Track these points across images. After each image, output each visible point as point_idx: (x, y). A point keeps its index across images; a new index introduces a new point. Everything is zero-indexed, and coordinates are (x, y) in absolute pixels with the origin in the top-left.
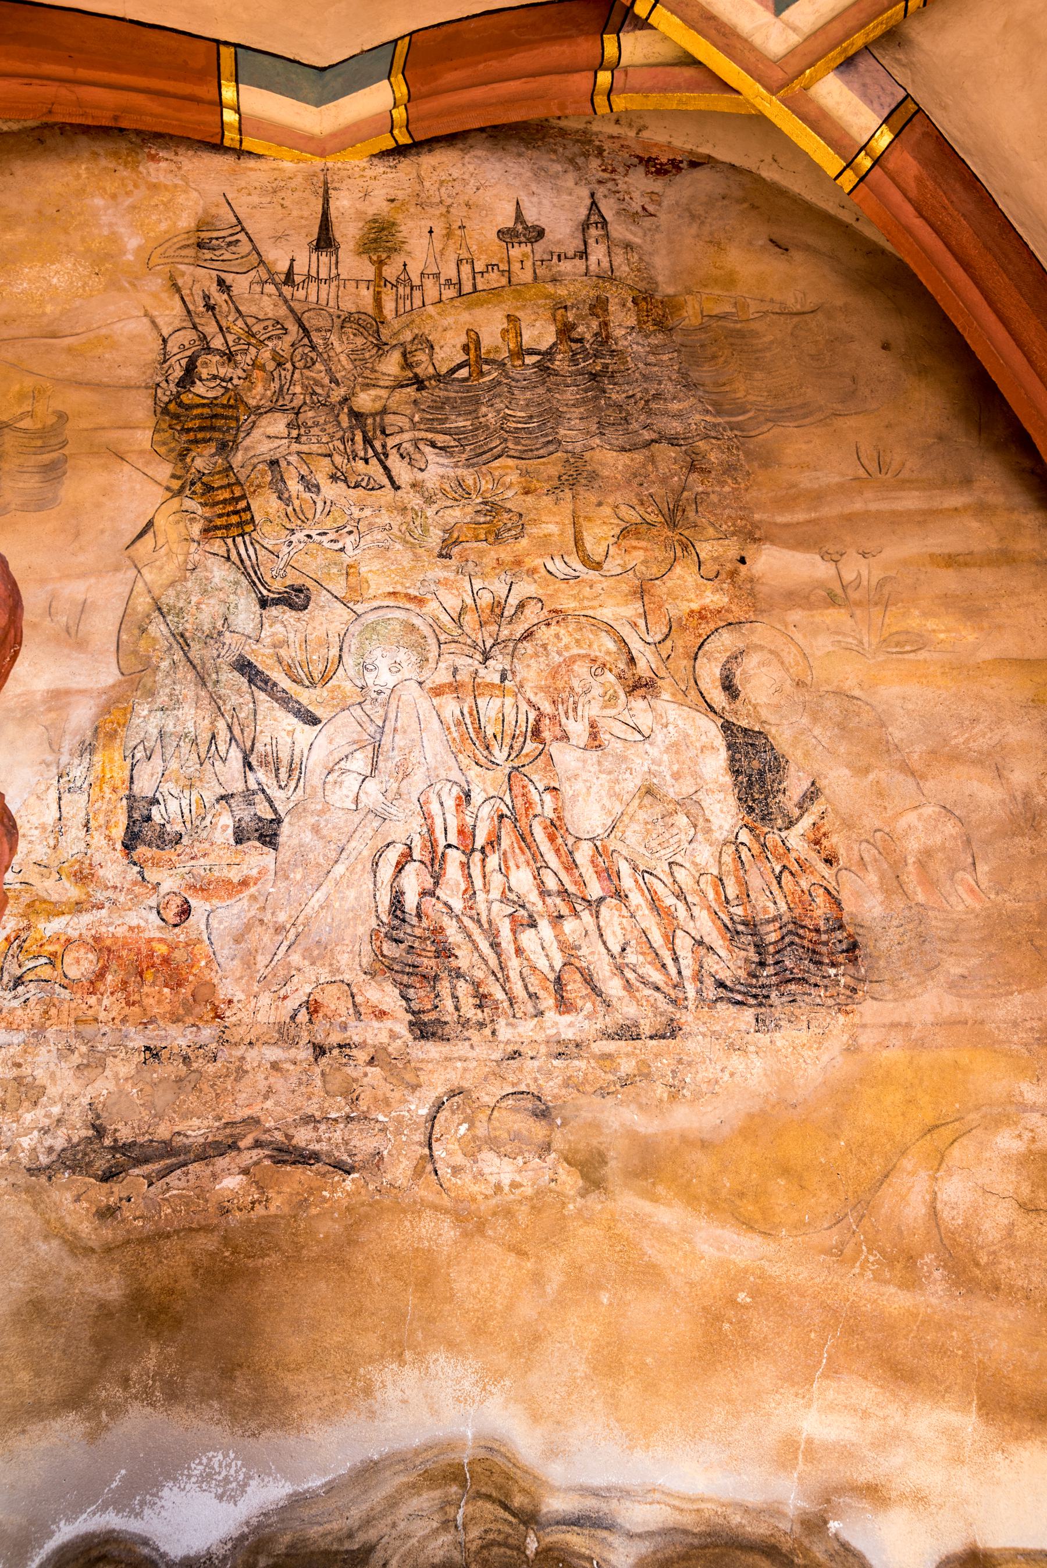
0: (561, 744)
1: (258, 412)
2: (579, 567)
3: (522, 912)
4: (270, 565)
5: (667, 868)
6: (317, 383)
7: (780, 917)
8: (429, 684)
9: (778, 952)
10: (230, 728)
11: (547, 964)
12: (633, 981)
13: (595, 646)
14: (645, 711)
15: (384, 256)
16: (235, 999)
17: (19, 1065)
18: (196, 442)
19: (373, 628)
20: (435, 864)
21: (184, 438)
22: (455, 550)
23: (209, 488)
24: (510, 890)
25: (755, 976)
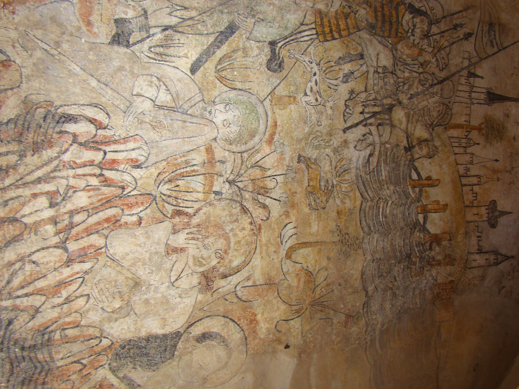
0: (170, 229)
1: (393, 49)
2: (288, 245)
3: (60, 199)
4: (297, 49)
5: (85, 293)
6: (410, 86)
7: (53, 361)
8: (214, 145)
9: (30, 359)
10: (191, 18)
11: (27, 213)
12: (14, 267)
13: (235, 253)
14: (191, 284)
15: (484, 132)
16: (15, 16)
18: (376, 11)
19: (254, 110)
20: (93, 144)
21: (378, 5)
22: (303, 166)
23: (347, 16)
24: (75, 192)
25: (15, 344)
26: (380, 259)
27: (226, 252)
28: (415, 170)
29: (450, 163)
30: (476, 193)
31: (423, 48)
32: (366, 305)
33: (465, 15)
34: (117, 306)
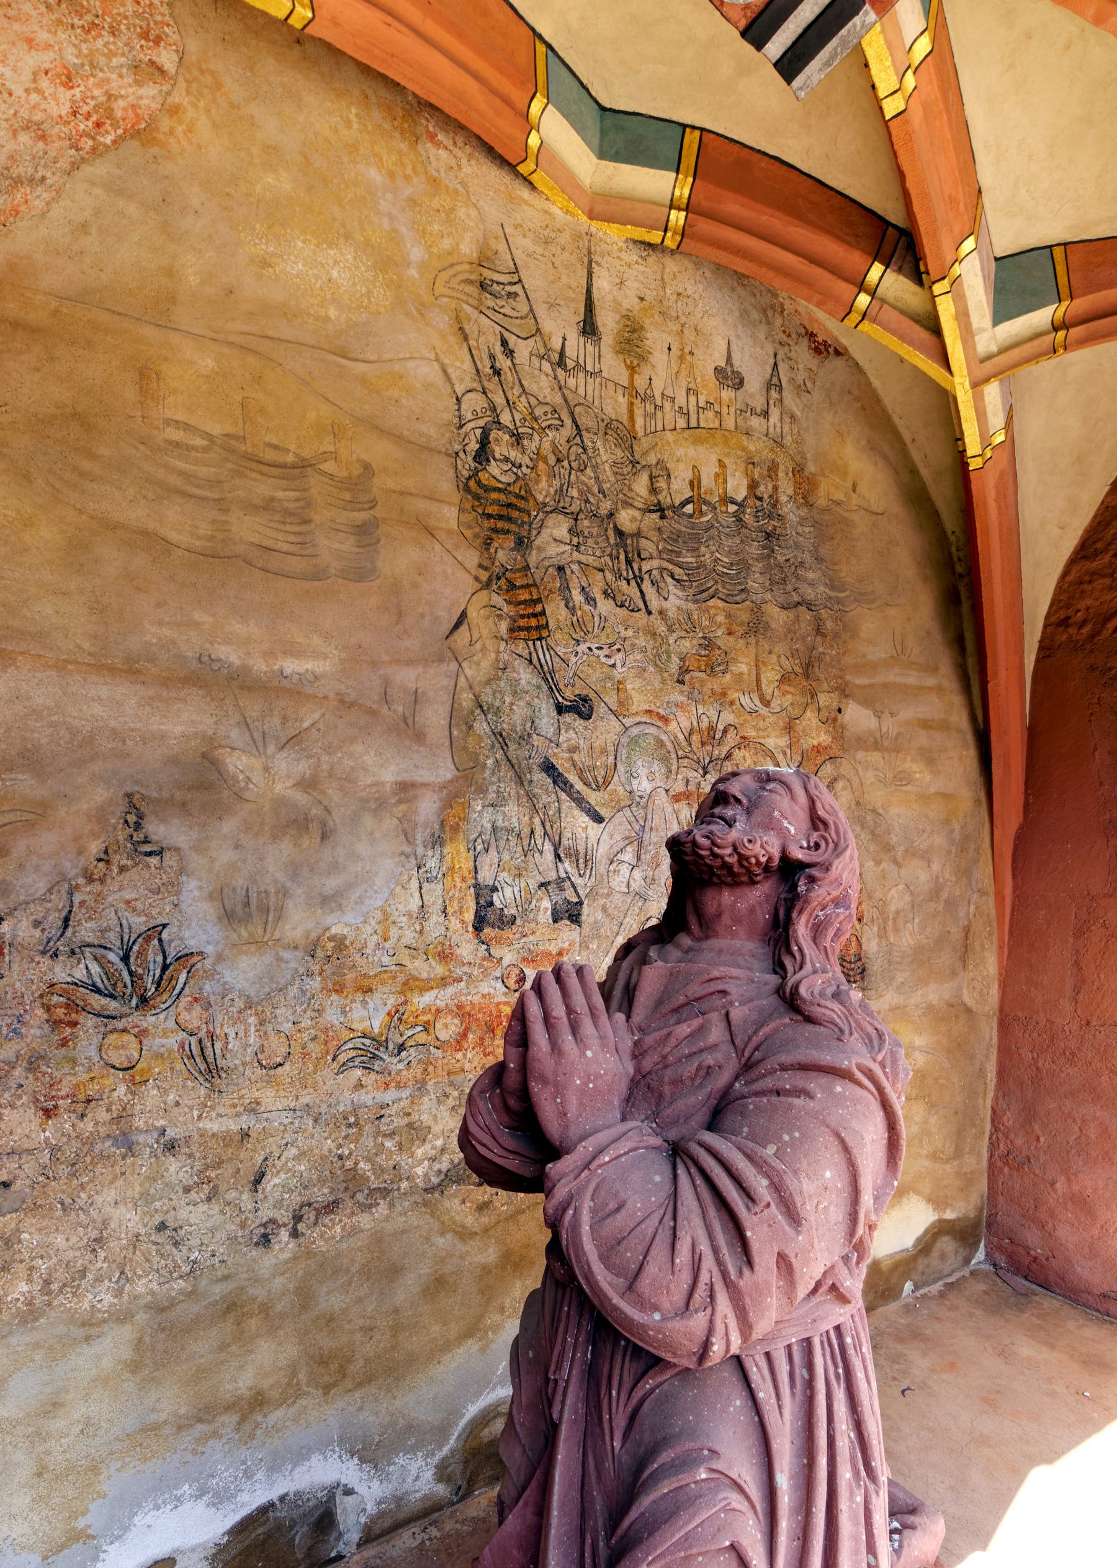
2: (758, 703)
8: (672, 793)
10: (543, 824)
15: (635, 362)
17: (409, 1114)
18: (496, 531)
19: (635, 741)
22: (687, 678)
23: (512, 586)
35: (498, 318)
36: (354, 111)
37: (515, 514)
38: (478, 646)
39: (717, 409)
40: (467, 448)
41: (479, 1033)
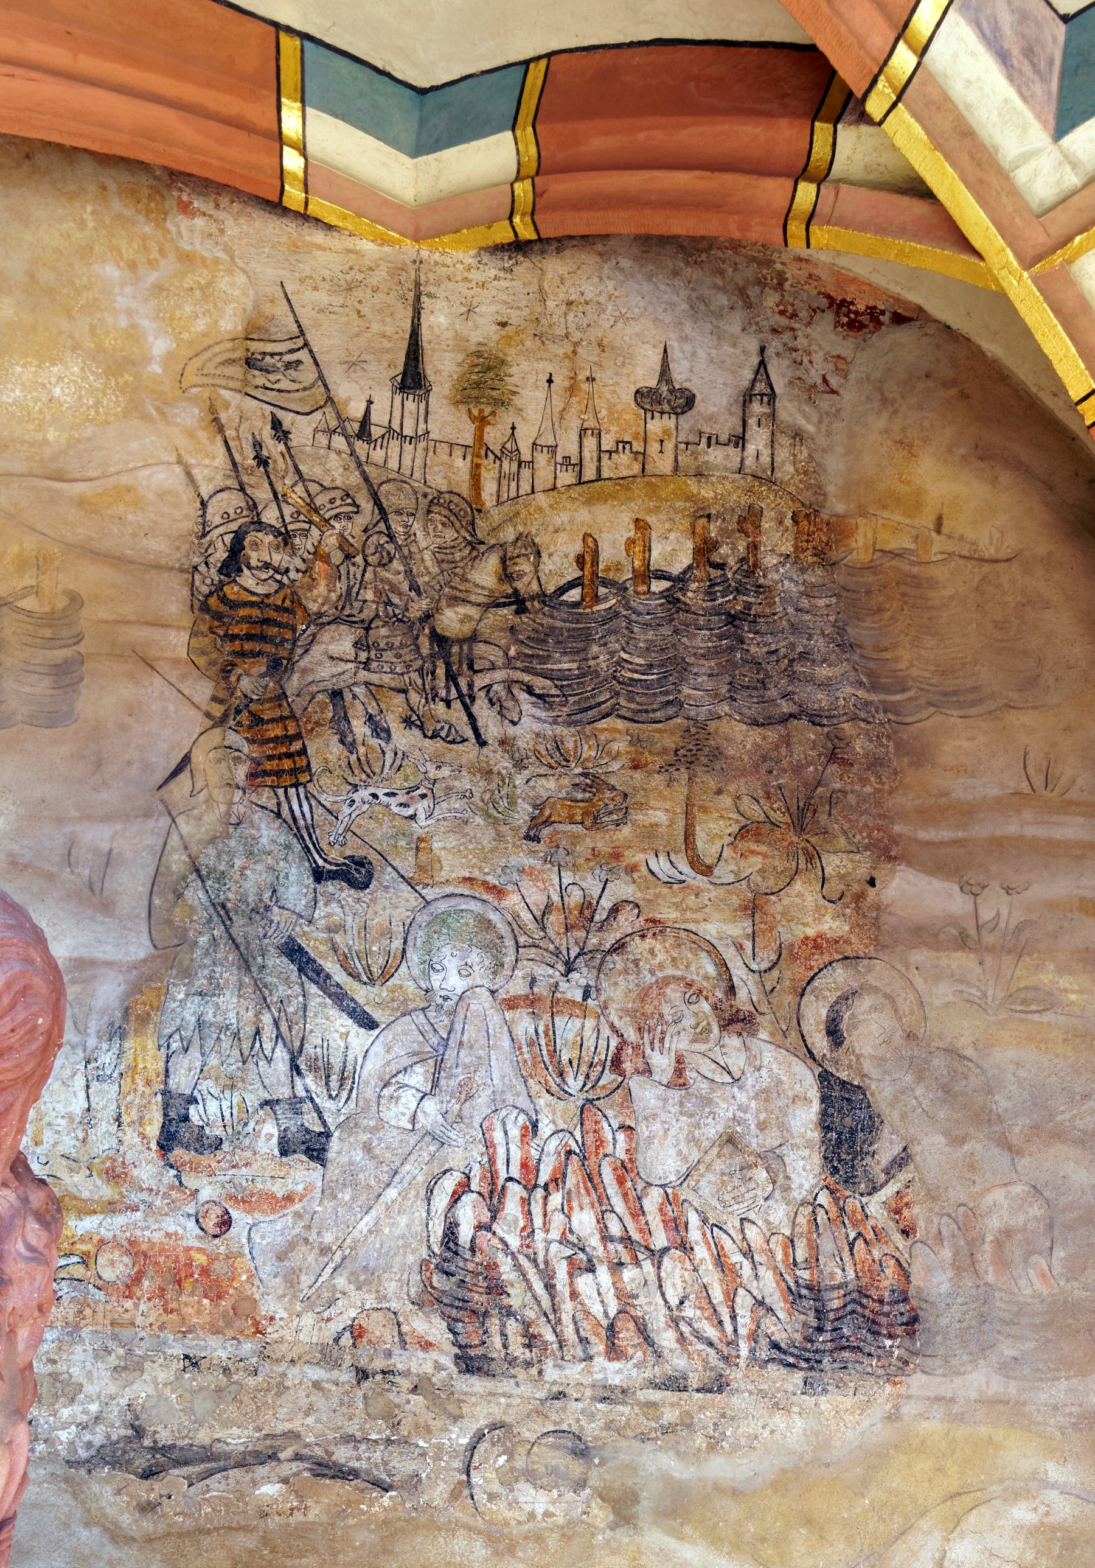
0: (642, 1078)
1: (318, 621)
2: (686, 869)
3: (581, 1255)
5: (738, 1225)
6: (394, 589)
7: (846, 1284)
8: (502, 995)
9: (837, 1319)
10: (276, 1023)
12: (687, 1334)
14: (739, 1050)
15: (488, 410)
16: (277, 1317)
17: (54, 1362)
18: (242, 654)
19: (441, 920)
20: (494, 1197)
21: (228, 648)
22: (546, 832)
23: (257, 720)
24: (571, 1231)
25: (811, 1341)
26: (730, 683)
27: (689, 985)
28: (562, 594)
29: (551, 506)
30: (617, 442)
31: (312, 550)
32: (815, 719)
33: (234, 433)
34: (764, 1174)
35: (270, 396)
36: (89, 209)
37: (273, 631)
38: (202, 796)
39: (638, 447)
40: (211, 559)
41: (158, 1281)
